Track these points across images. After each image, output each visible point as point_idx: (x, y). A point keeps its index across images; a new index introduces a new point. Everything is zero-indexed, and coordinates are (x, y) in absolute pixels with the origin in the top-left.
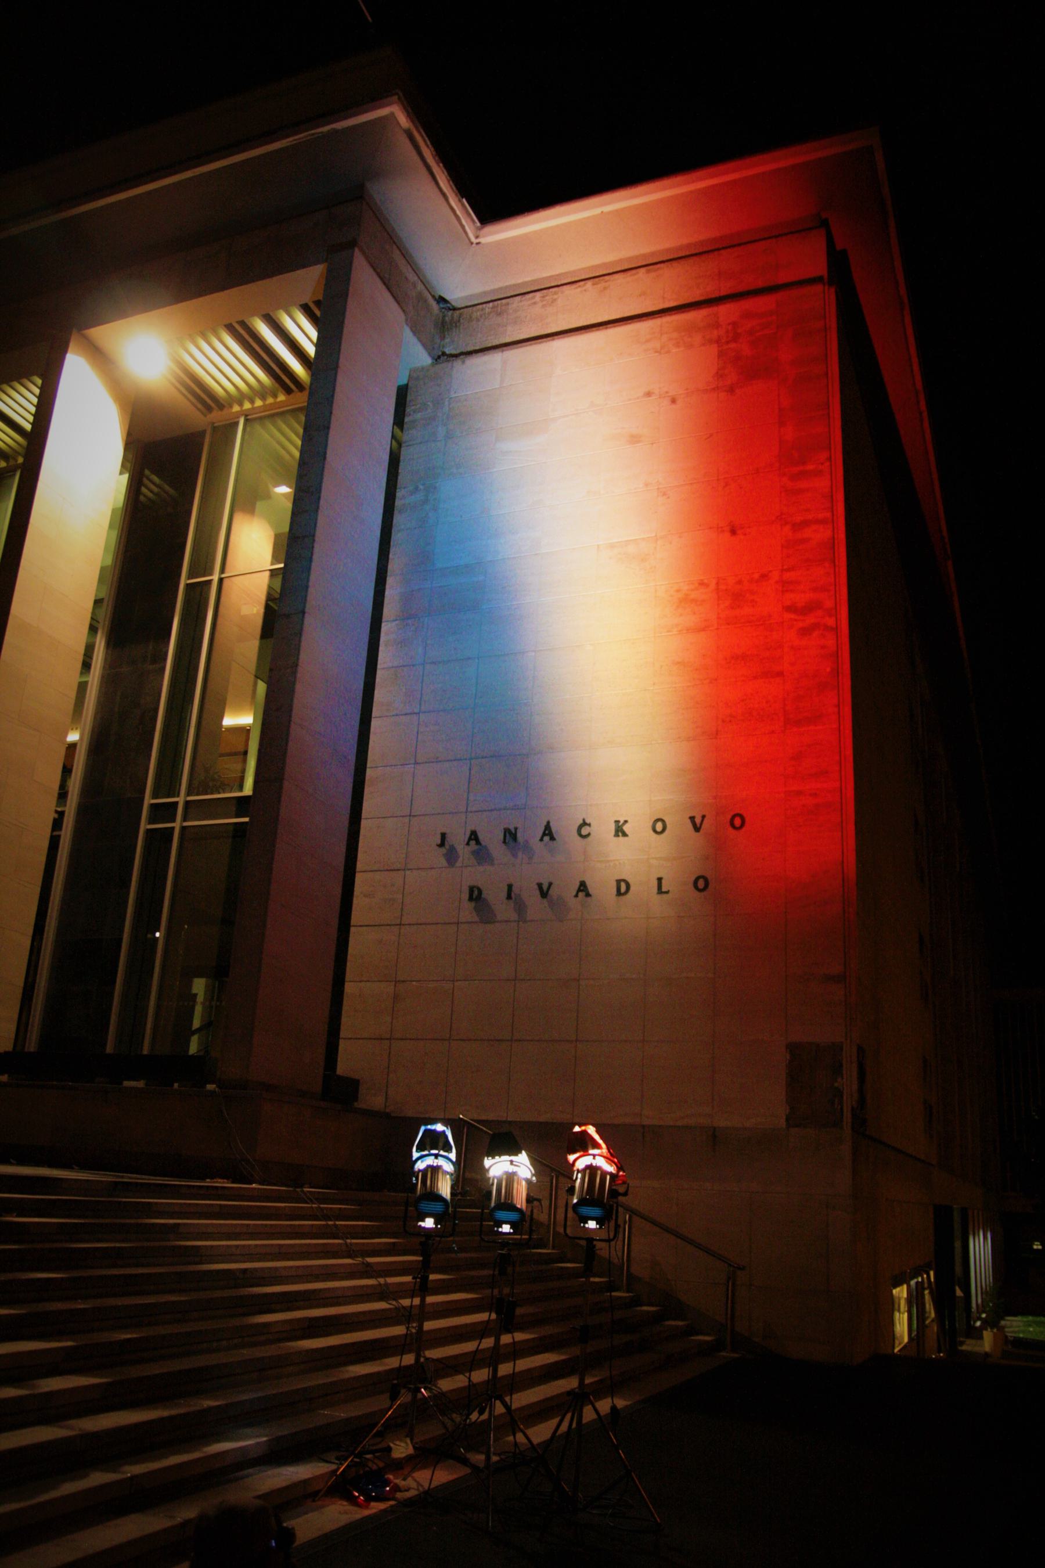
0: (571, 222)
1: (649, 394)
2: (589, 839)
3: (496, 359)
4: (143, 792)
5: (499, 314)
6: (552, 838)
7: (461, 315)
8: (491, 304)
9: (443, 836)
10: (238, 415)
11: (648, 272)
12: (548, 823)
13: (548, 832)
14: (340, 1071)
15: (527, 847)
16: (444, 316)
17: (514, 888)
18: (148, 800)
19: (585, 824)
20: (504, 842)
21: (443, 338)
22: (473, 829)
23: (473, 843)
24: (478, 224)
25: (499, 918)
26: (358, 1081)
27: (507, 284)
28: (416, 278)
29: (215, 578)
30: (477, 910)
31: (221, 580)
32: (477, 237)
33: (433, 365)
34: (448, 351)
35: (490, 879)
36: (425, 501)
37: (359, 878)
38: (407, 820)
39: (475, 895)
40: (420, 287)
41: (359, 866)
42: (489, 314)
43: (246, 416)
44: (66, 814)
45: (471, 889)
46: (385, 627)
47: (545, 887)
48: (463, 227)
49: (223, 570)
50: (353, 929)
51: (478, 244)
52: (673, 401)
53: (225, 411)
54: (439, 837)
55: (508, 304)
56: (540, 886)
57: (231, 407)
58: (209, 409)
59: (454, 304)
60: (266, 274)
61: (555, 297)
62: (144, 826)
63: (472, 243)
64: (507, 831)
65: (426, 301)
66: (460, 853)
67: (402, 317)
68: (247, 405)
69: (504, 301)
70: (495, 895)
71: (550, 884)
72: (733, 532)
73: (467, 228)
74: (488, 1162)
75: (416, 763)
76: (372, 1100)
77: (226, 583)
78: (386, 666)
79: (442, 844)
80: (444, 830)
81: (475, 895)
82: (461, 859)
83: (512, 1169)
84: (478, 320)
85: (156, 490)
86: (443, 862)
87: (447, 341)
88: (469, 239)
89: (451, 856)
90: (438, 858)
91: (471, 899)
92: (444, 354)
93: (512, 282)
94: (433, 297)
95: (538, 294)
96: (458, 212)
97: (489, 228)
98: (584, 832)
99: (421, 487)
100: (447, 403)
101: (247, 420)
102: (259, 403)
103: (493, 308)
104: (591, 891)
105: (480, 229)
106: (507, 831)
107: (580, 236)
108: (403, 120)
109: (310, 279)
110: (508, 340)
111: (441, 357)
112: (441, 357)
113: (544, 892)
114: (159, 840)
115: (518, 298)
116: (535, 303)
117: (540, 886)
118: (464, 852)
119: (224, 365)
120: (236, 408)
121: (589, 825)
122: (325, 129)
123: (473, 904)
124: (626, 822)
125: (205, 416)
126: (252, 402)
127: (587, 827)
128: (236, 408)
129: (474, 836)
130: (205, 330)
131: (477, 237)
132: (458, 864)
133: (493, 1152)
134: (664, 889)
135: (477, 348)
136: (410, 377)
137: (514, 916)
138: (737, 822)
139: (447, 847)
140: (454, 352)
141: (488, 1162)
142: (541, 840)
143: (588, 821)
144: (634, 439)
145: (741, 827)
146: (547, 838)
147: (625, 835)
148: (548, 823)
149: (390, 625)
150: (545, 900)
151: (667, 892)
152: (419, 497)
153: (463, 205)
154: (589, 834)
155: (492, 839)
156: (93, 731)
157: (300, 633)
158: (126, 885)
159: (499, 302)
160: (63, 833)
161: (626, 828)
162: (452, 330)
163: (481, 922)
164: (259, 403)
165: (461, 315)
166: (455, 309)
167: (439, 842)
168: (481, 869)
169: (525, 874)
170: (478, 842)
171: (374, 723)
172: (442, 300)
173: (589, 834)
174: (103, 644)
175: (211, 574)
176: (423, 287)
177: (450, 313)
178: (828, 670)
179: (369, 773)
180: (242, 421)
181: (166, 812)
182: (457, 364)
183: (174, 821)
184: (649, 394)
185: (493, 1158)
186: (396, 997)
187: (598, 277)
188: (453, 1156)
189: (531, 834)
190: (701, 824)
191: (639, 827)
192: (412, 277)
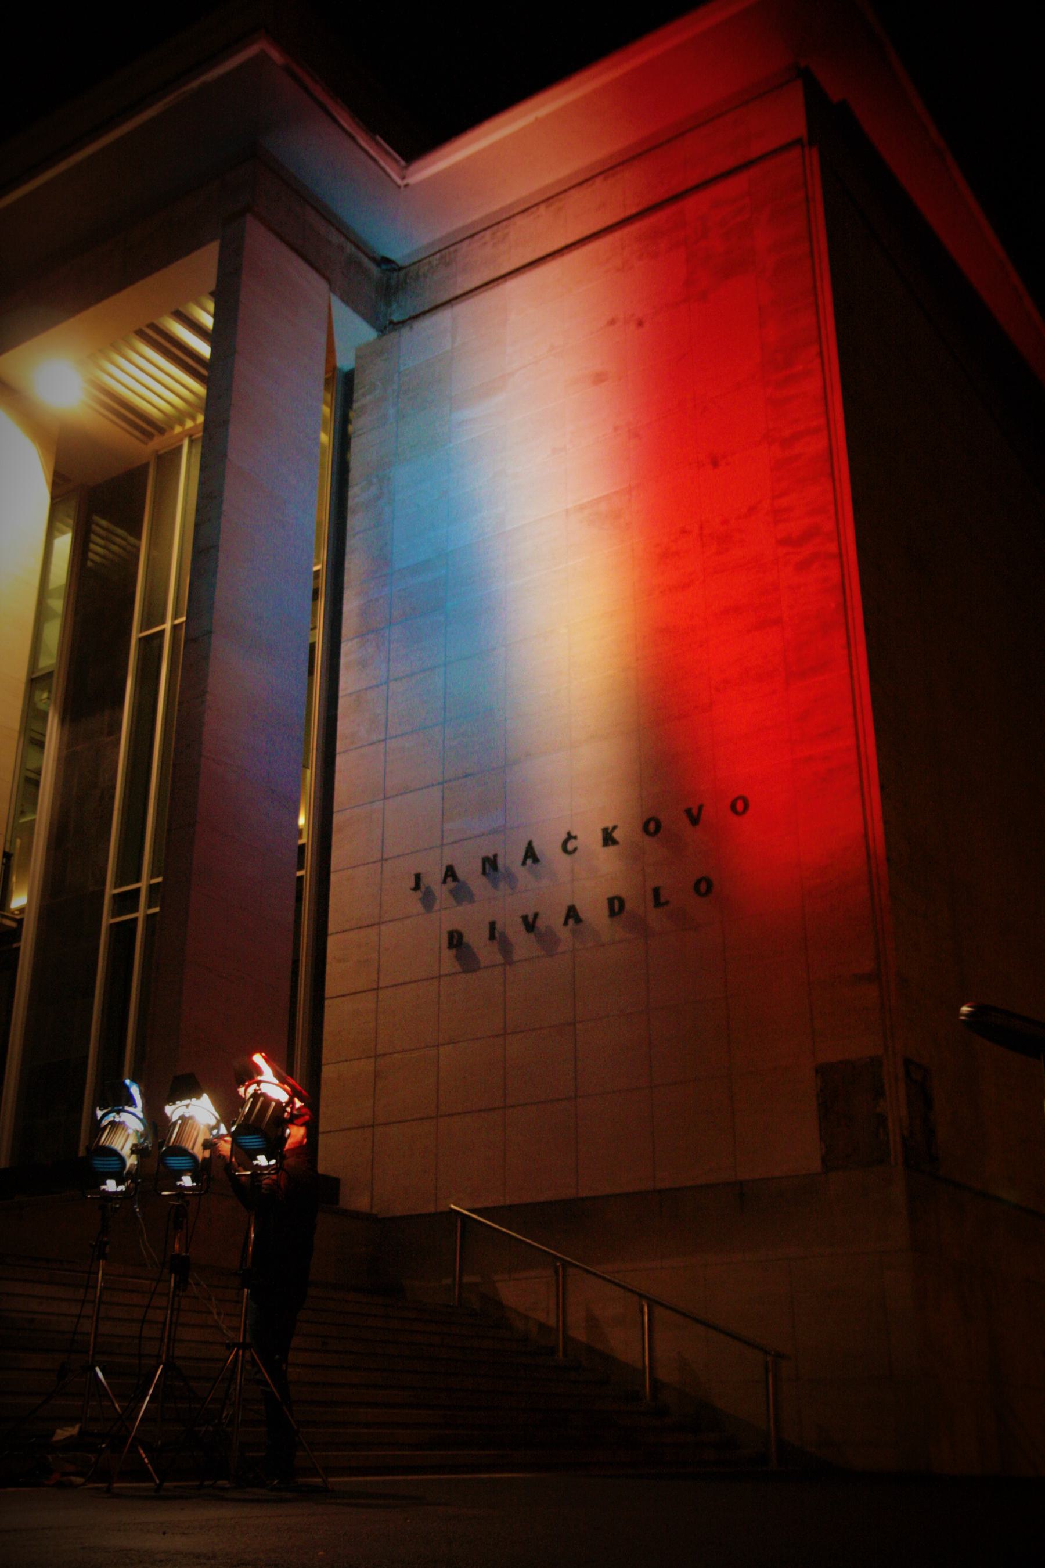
0: (505, 138)
2: (577, 854)
3: (444, 317)
4: (104, 884)
5: (447, 265)
6: (536, 860)
7: (406, 275)
8: (438, 255)
9: (418, 877)
11: (606, 179)
12: (530, 844)
13: (530, 854)
14: (321, 1169)
15: (510, 878)
16: (389, 279)
17: (498, 926)
18: (110, 891)
19: (570, 837)
20: (484, 872)
21: (388, 305)
22: (450, 863)
23: (449, 879)
24: (403, 163)
25: (482, 965)
26: (337, 1181)
27: (454, 227)
28: (343, 239)
30: (458, 958)
32: (403, 178)
33: (379, 338)
34: (395, 318)
35: (470, 919)
36: (379, 497)
37: (331, 942)
38: (379, 864)
39: (456, 940)
40: (350, 248)
41: (332, 927)
42: (437, 265)
43: (191, 436)
44: (25, 923)
45: (451, 934)
46: (345, 647)
47: (695, 811)
48: (384, 171)
50: (327, 1003)
51: (406, 186)
52: (640, 324)
53: (167, 435)
54: (413, 878)
55: (456, 251)
57: (172, 429)
58: (150, 436)
59: (400, 263)
60: (165, 262)
61: (506, 231)
62: (107, 920)
63: (399, 187)
64: (486, 860)
65: (359, 264)
66: (437, 893)
67: (323, 285)
68: (189, 424)
69: (452, 249)
70: (476, 939)
72: (715, 464)
73: (388, 169)
74: (169, 1109)
75: (385, 798)
76: (358, 1201)
78: (349, 691)
79: (417, 887)
80: (419, 870)
81: (456, 940)
82: (438, 901)
83: (199, 1115)
84: (425, 276)
85: (123, 543)
86: (419, 908)
87: (394, 306)
88: (395, 183)
89: (428, 900)
90: (413, 903)
91: (451, 945)
92: (391, 322)
93: (460, 224)
94: (373, 259)
95: (488, 233)
96: (373, 153)
97: (415, 166)
98: (570, 847)
99: (375, 480)
100: (396, 378)
103: (442, 257)
104: (582, 916)
105: (406, 168)
106: (486, 860)
107: (520, 151)
108: (275, 55)
110: (459, 292)
111: (386, 327)
112: (386, 327)
113: (530, 924)
114: (124, 933)
115: (466, 242)
116: (485, 243)
117: (688, 812)
118: (441, 891)
119: (157, 386)
120: (178, 429)
121: (575, 838)
122: (195, 84)
123: (454, 952)
124: (615, 828)
125: (146, 444)
126: (194, 419)
127: (573, 841)
128: (178, 429)
129: (450, 873)
130: (114, 343)
131: (403, 178)
132: (436, 907)
133: (172, 1099)
134: (662, 900)
135: (427, 308)
136: (358, 357)
137: (499, 958)
139: (423, 889)
140: (400, 319)
141: (169, 1109)
142: (524, 863)
143: (573, 834)
144: (599, 378)
146: (529, 861)
147: (615, 842)
148: (530, 844)
149: (350, 644)
150: (532, 935)
151: (667, 903)
152: (374, 490)
153: (378, 144)
154: (575, 849)
155: (469, 870)
156: (51, 824)
157: (206, 657)
158: (89, 992)
159: (446, 252)
160: (22, 944)
161: (616, 835)
162: (393, 293)
163: (464, 972)
165: (406, 275)
166: (401, 269)
167: (413, 885)
168: (460, 908)
169: (506, 906)
170: (455, 878)
171: (339, 760)
172: (386, 261)
173: (575, 849)
174: (56, 721)
175: (163, 622)
176: (353, 249)
177: (395, 274)
178: (833, 605)
179: (337, 819)
180: (186, 443)
181: (127, 902)
182: (405, 332)
183: (137, 911)
185: (174, 1103)
186: (377, 1075)
187: (550, 199)
189: (512, 859)
191: (589, 838)
192: (335, 238)
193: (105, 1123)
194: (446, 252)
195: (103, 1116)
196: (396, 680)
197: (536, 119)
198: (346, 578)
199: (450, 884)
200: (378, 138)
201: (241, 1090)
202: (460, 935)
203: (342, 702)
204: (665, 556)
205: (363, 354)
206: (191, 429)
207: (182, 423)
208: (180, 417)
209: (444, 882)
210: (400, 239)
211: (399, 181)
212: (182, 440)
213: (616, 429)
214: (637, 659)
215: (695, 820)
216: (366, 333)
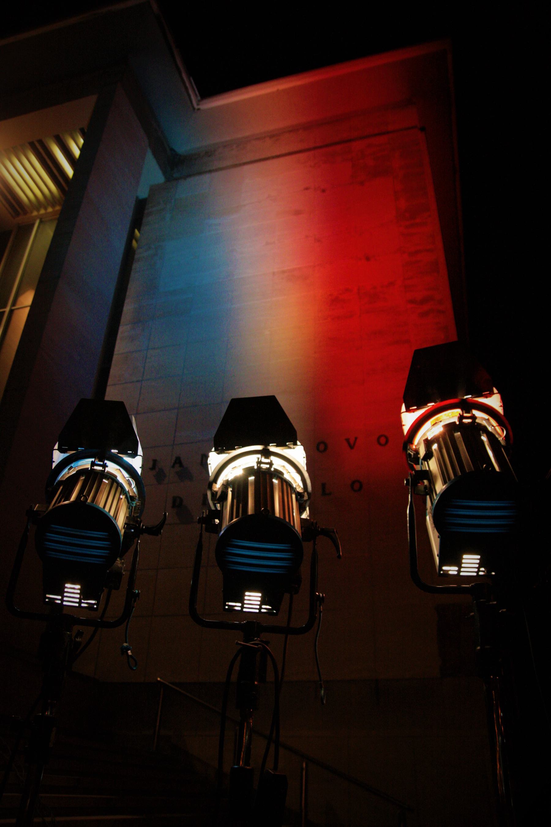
1: (307, 189)
5: (209, 156)
10: (37, 217)
23: (177, 466)
24: (199, 98)
29: (7, 309)
31: (11, 312)
32: (198, 105)
45: (175, 499)
47: (352, 441)
49: (14, 304)
52: (324, 191)
56: (348, 440)
57: (32, 213)
58: (17, 214)
63: (194, 109)
68: (42, 211)
71: (356, 439)
77: (16, 312)
91: (174, 506)
97: (206, 101)
101: (41, 222)
102: (50, 210)
109: (86, 105)
111: (169, 179)
117: (348, 440)
120: (35, 213)
128: (35, 213)
129: (178, 461)
131: (198, 105)
138: (383, 440)
144: (297, 213)
145: (387, 442)
159: (209, 153)
164: (50, 210)
184: (307, 189)
188: (137, 463)
190: (354, 444)
193: (66, 474)
194: (209, 153)
195: (63, 464)
196: (152, 349)
197: (278, 90)
198: (128, 293)
199: (178, 468)
200: (191, 78)
201: (494, 401)
202: (181, 500)
203: (115, 358)
204: (334, 301)
205: (154, 190)
206: (42, 215)
207: (38, 210)
208: (39, 205)
209: (173, 466)
210: (183, 143)
211: (196, 107)
212: (35, 220)
213: (307, 237)
214: (315, 353)
215: (351, 447)
216: (159, 177)
